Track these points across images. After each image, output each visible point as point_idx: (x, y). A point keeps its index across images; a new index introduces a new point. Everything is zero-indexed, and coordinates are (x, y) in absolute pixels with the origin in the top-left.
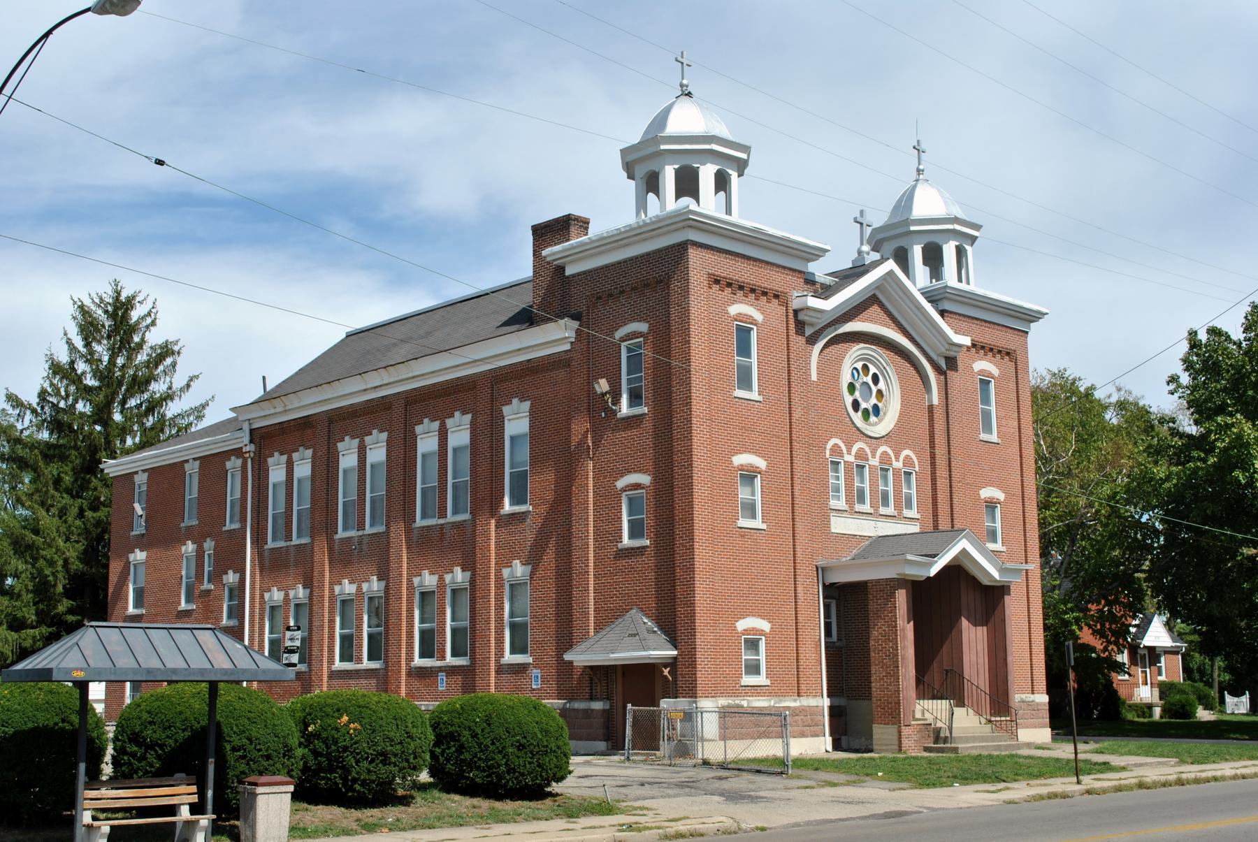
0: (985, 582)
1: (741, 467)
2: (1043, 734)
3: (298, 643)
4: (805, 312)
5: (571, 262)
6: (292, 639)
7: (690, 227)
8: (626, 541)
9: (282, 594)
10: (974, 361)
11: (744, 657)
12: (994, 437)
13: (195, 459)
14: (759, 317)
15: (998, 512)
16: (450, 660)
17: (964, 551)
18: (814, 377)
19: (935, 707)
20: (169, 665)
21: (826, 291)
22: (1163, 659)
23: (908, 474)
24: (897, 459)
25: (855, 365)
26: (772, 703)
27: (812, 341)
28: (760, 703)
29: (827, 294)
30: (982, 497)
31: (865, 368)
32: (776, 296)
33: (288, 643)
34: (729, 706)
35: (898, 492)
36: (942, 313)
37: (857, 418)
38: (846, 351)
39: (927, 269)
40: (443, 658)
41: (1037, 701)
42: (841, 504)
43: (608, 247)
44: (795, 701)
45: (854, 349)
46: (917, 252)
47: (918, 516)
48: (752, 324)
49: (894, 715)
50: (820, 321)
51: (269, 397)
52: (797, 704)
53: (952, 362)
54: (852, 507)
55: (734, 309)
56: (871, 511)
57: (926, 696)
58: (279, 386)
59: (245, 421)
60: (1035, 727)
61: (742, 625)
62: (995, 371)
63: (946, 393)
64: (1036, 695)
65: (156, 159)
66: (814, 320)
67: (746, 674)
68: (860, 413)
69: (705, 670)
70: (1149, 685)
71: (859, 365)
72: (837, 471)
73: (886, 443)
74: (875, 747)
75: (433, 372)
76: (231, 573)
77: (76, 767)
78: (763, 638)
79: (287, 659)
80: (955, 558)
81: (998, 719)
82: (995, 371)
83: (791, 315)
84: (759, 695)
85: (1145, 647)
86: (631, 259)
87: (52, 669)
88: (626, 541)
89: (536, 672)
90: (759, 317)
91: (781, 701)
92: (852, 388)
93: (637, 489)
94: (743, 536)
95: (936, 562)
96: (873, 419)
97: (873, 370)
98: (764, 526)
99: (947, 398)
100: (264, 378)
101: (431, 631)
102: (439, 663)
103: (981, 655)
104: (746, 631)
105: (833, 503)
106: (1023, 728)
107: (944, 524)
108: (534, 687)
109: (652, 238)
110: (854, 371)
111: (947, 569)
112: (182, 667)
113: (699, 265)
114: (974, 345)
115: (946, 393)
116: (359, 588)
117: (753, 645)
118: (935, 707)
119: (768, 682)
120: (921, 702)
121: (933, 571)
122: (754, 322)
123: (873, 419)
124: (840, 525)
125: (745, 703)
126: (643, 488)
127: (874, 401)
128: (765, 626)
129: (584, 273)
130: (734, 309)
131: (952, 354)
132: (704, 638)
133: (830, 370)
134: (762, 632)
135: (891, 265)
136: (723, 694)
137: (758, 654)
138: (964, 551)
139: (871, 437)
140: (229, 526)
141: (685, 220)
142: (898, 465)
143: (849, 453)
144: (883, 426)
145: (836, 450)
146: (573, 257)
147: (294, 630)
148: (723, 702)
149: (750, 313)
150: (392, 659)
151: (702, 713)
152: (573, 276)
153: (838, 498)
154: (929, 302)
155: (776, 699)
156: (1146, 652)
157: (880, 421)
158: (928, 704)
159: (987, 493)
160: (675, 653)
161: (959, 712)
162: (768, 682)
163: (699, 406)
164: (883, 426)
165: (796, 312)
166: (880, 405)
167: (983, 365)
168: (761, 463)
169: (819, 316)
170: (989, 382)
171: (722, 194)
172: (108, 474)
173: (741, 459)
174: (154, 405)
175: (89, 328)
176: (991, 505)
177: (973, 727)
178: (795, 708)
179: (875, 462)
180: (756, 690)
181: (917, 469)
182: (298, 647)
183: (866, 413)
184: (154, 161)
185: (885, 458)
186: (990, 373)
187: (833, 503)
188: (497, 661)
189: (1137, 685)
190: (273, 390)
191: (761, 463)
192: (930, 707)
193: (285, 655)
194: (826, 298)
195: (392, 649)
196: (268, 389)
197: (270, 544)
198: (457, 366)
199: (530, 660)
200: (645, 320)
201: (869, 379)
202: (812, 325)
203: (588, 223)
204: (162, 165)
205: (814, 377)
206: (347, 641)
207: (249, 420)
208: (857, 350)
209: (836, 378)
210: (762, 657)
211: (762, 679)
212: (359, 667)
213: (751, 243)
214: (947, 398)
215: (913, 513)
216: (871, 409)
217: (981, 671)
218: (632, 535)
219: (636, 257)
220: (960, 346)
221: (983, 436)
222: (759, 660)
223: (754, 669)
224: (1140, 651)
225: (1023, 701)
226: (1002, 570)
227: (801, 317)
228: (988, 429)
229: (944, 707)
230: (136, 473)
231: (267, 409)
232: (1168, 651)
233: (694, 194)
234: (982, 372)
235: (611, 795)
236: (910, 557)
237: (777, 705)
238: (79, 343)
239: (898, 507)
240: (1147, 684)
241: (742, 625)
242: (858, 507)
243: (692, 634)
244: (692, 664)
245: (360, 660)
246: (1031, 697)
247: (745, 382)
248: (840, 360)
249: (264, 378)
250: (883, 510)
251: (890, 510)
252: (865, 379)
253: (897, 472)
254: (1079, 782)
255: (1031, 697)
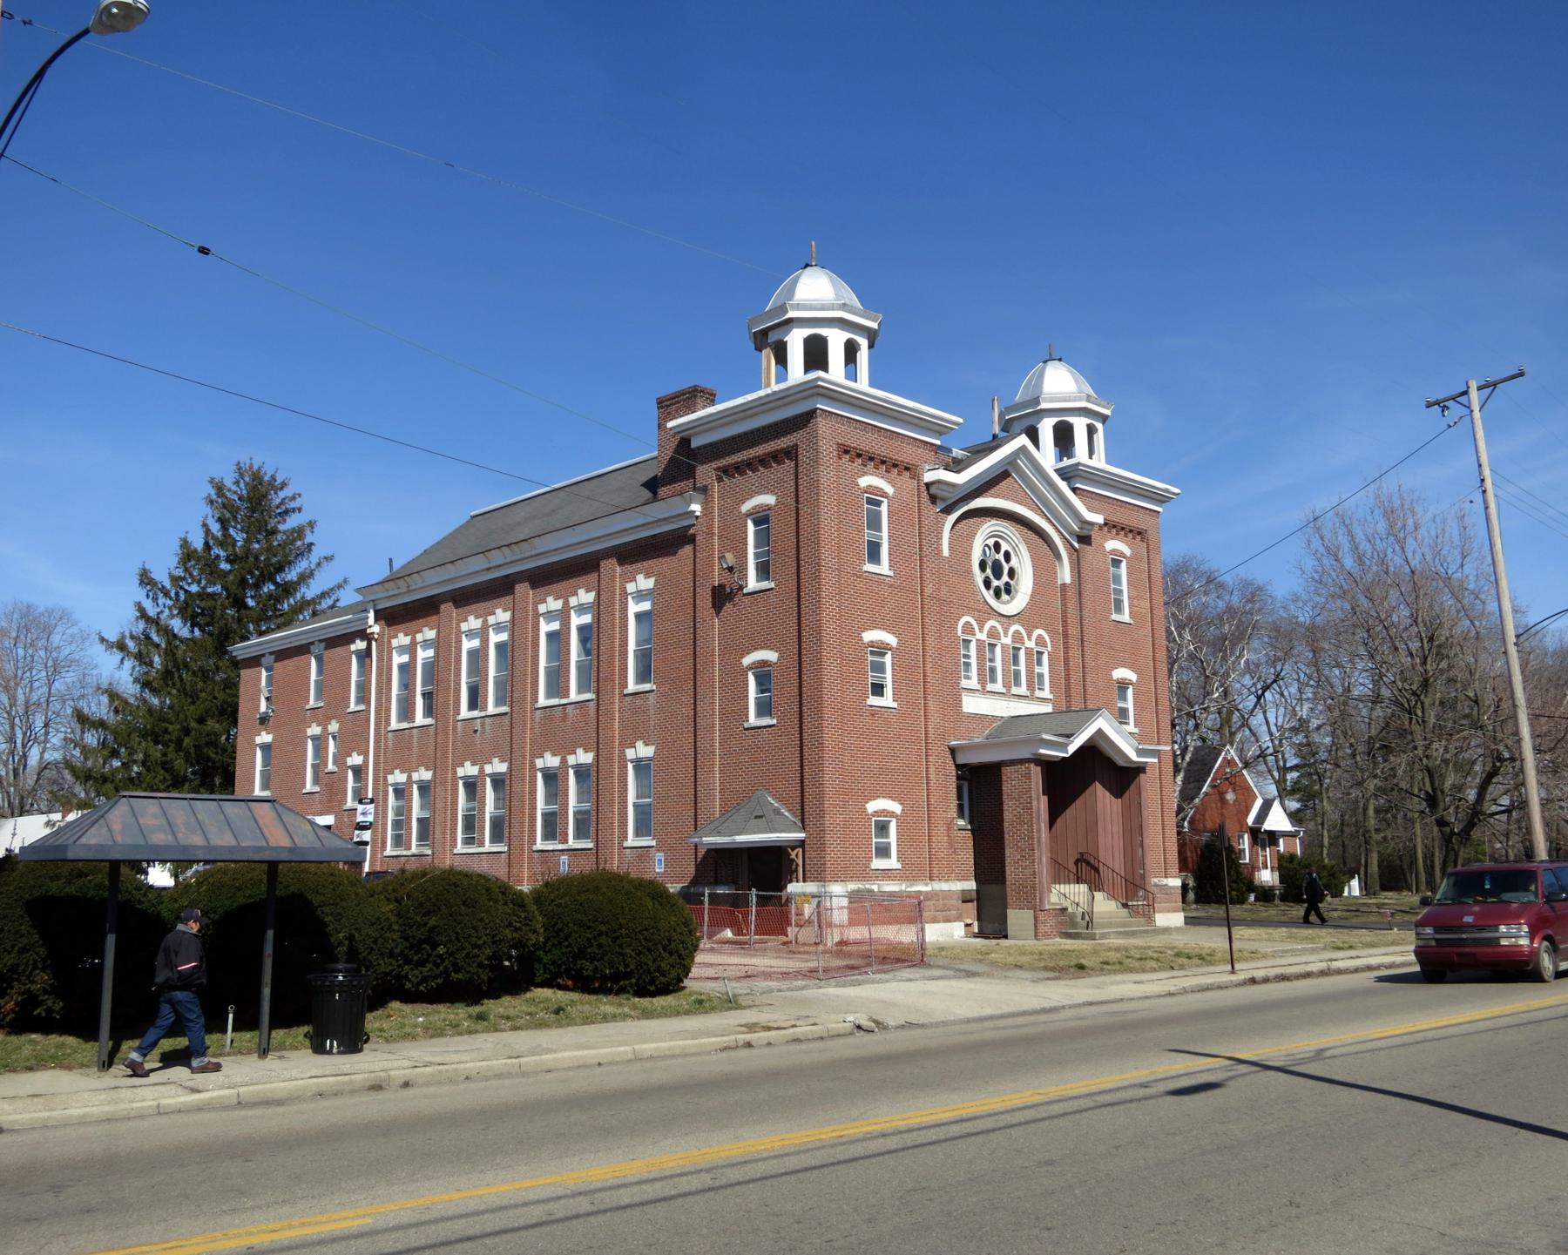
0: (1122, 763)
1: (871, 644)
2: (1175, 919)
3: (370, 818)
4: (937, 486)
5: (696, 434)
6: (364, 814)
7: (819, 394)
8: (753, 720)
9: (405, 776)
10: (1106, 541)
11: (874, 840)
12: (1126, 617)
13: (320, 641)
14: (889, 490)
15: (1130, 692)
16: (572, 843)
17: (1100, 732)
18: (946, 552)
19: (1072, 891)
20: (273, 843)
21: (957, 465)
22: (1281, 841)
23: (1040, 653)
24: (1030, 638)
25: (987, 542)
26: (903, 887)
27: (948, 510)
28: (891, 887)
29: (959, 468)
30: (1115, 678)
31: (997, 547)
32: (907, 469)
33: (360, 819)
34: (859, 891)
35: (1030, 672)
36: (1074, 490)
37: (989, 596)
38: (978, 527)
39: (1057, 449)
40: (566, 841)
41: (1170, 884)
42: (973, 682)
43: (733, 417)
44: (927, 885)
45: (986, 525)
46: (1046, 428)
47: (1051, 697)
48: (882, 496)
49: (1033, 900)
50: (949, 495)
51: (393, 579)
52: (929, 888)
53: (1085, 539)
54: (984, 687)
55: (865, 481)
56: (1004, 691)
57: (1062, 880)
58: (402, 567)
59: (369, 602)
60: (1168, 911)
61: (872, 806)
62: (1127, 551)
63: (1079, 572)
64: (1170, 879)
65: (200, 247)
66: (945, 494)
67: (877, 856)
68: (992, 591)
69: (834, 851)
70: (1269, 869)
71: (991, 542)
72: (967, 648)
73: (1019, 622)
74: (1009, 933)
75: (556, 550)
76: (355, 754)
77: (264, 932)
78: (894, 820)
79: (358, 836)
80: (1091, 739)
81: (1135, 903)
82: (1127, 551)
83: (923, 489)
84: (889, 878)
85: (1265, 831)
86: (758, 430)
87: (66, 846)
88: (753, 720)
89: (660, 855)
90: (889, 490)
91: (912, 885)
92: (983, 566)
93: (763, 667)
94: (873, 715)
95: (1072, 742)
96: (1005, 597)
97: (1004, 547)
98: (895, 705)
99: (1079, 577)
100: (391, 560)
101: (554, 814)
102: (561, 847)
103: (1116, 837)
104: (876, 813)
105: (964, 683)
106: (1160, 912)
107: (1077, 704)
108: (657, 870)
109: (780, 407)
110: (987, 549)
111: (1082, 750)
112: (283, 844)
113: (826, 434)
114: (1106, 524)
115: (1079, 572)
116: (482, 770)
117: (882, 828)
118: (1077, 890)
119: (899, 866)
120: (1057, 886)
121: (1072, 749)
122: (885, 495)
123: (1005, 597)
124: (973, 704)
125: (875, 888)
126: (770, 666)
127: (1005, 578)
128: (896, 807)
129: (711, 445)
130: (865, 481)
131: (1085, 533)
132: (833, 820)
133: (962, 545)
134: (892, 814)
135: (1023, 440)
136: (851, 879)
137: (887, 836)
138: (1100, 732)
139: (1003, 616)
140: (353, 707)
141: (813, 390)
142: (1031, 644)
143: (981, 630)
144: (1017, 604)
145: (968, 628)
146: (701, 428)
147: (367, 804)
148: (852, 886)
149: (881, 486)
150: (515, 842)
151: (831, 897)
152: (699, 448)
153: (968, 678)
154: (1063, 479)
155: (908, 883)
156: (1266, 836)
157: (1012, 599)
158: (1064, 888)
159: (1121, 673)
160: (804, 835)
161: (1099, 896)
162: (899, 866)
163: (828, 579)
164: (1017, 604)
165: (928, 485)
166: (1012, 582)
167: (1113, 544)
168: (892, 640)
169: (951, 490)
170: (1121, 561)
171: (852, 365)
172: (235, 657)
173: (870, 636)
174: (288, 589)
175: (227, 512)
176: (1123, 685)
177: (1110, 912)
178: (927, 893)
179: (1007, 640)
180: (886, 874)
181: (1049, 649)
182: (371, 823)
183: (997, 594)
184: (196, 249)
185: (1017, 637)
186: (1122, 553)
187: (964, 683)
188: (620, 844)
189: (1259, 869)
190: (398, 571)
191: (892, 640)
192: (1067, 891)
193: (357, 832)
194: (958, 472)
195: (515, 832)
196: (395, 569)
197: (394, 725)
198: (581, 543)
199: (653, 843)
200: (773, 492)
201: (1001, 557)
202: (943, 499)
203: (715, 395)
204: (207, 254)
205: (946, 552)
206: (471, 824)
207: (373, 601)
208: (989, 526)
209: (968, 554)
210: (893, 838)
211: (892, 863)
212: (481, 850)
213: (881, 414)
214: (1079, 577)
215: (1046, 694)
216: (1003, 588)
217: (1117, 854)
218: (759, 714)
219: (764, 428)
220: (1092, 524)
221: (1115, 617)
222: (889, 843)
223: (883, 852)
224: (1260, 836)
225: (1156, 885)
226: (1140, 752)
227: (933, 490)
228: (1119, 609)
229: (1082, 890)
230: (263, 655)
231: (392, 589)
232: (1285, 834)
233: (824, 366)
234: (1114, 552)
235: (735, 988)
236: (1045, 736)
237: (909, 889)
238: (215, 527)
239: (1030, 687)
240: (1267, 868)
241: (872, 806)
242: (990, 687)
243: (821, 815)
244: (822, 847)
245: (482, 844)
246: (1165, 881)
247: (874, 555)
248: (972, 536)
249: (391, 560)
250: (1015, 690)
251: (1023, 690)
252: (997, 557)
253: (1029, 652)
254: (1233, 971)
255: (1165, 881)
